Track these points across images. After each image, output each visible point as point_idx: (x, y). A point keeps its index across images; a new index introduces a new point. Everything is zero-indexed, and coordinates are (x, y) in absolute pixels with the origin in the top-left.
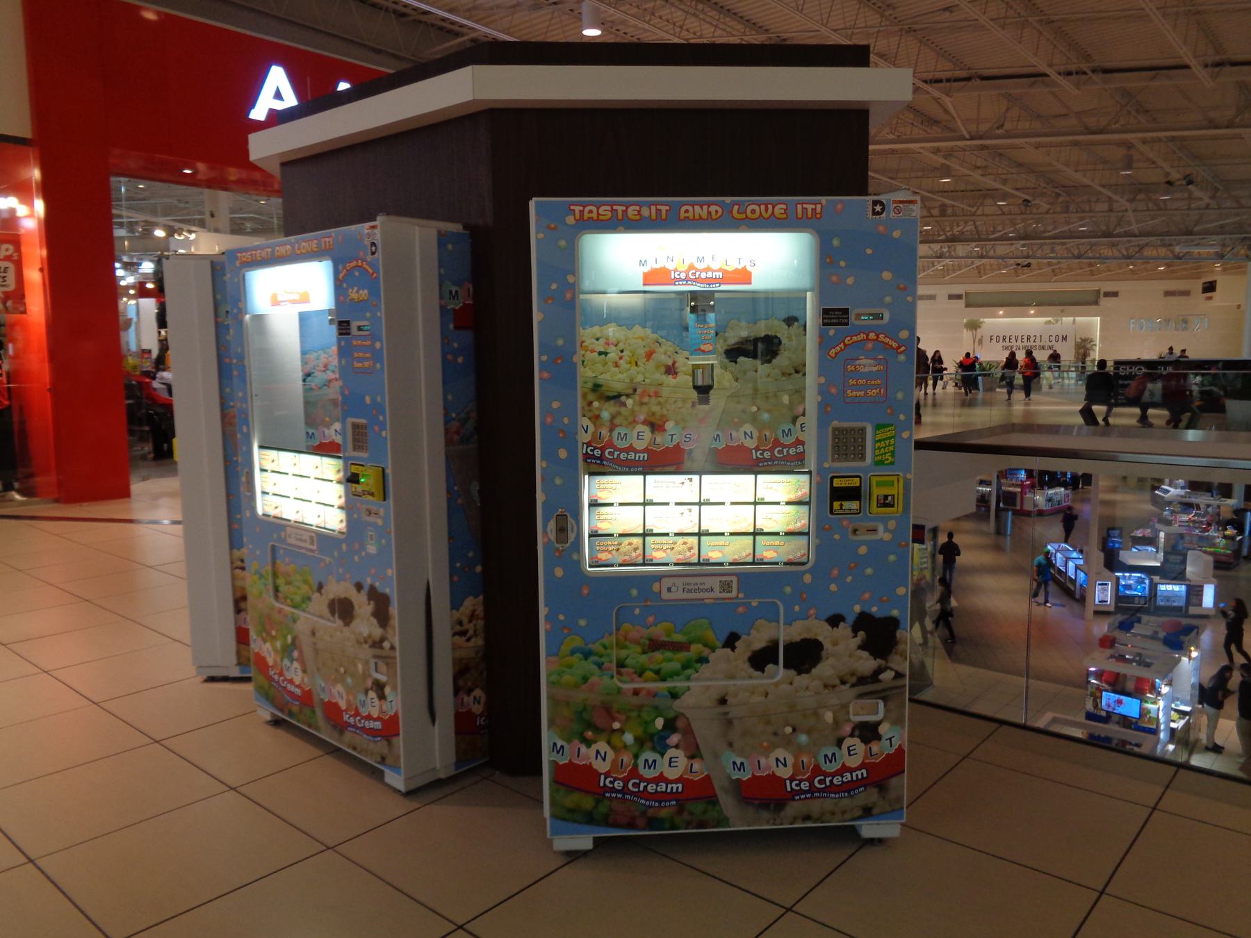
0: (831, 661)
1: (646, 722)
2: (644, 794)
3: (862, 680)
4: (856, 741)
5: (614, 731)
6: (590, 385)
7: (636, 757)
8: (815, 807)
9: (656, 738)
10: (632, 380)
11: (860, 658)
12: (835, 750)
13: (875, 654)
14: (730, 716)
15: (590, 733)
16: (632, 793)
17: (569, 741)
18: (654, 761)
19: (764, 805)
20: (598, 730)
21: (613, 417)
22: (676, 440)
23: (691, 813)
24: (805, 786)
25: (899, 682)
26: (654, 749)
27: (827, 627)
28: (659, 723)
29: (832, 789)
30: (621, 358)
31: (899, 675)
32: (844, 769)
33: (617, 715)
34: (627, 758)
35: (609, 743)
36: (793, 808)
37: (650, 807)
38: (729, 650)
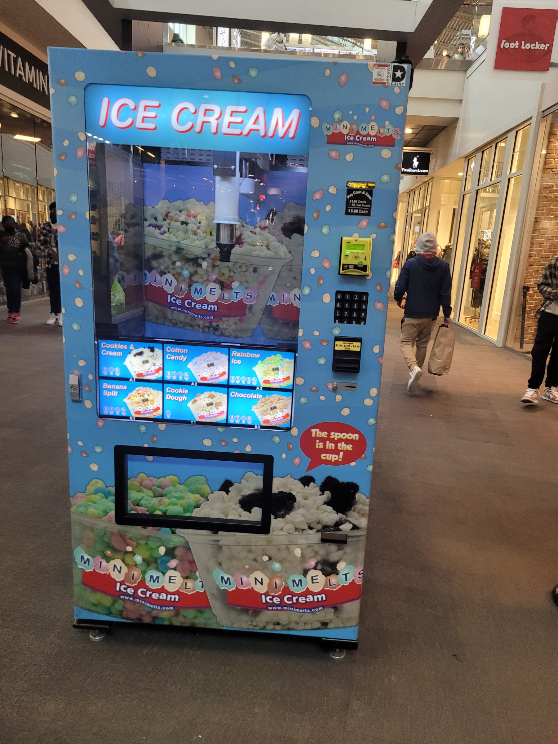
0: (301, 511)
1: (152, 549)
2: (150, 600)
3: (325, 527)
4: (319, 573)
5: (127, 553)
6: (174, 248)
7: (144, 573)
8: (283, 617)
9: (159, 561)
10: (207, 247)
11: (326, 511)
12: (302, 577)
13: (338, 510)
14: (220, 543)
15: (109, 552)
16: (140, 598)
17: (93, 557)
18: (158, 577)
19: (245, 610)
20: (115, 551)
21: (192, 275)
22: (240, 296)
23: (184, 617)
24: (276, 600)
25: (356, 533)
26: (157, 569)
27: (300, 485)
28: (162, 550)
29: (297, 605)
30: (198, 228)
31: (355, 527)
32: (308, 592)
33: (129, 541)
34: (136, 573)
35: (123, 561)
36: (266, 617)
37: (153, 609)
38: (224, 493)
